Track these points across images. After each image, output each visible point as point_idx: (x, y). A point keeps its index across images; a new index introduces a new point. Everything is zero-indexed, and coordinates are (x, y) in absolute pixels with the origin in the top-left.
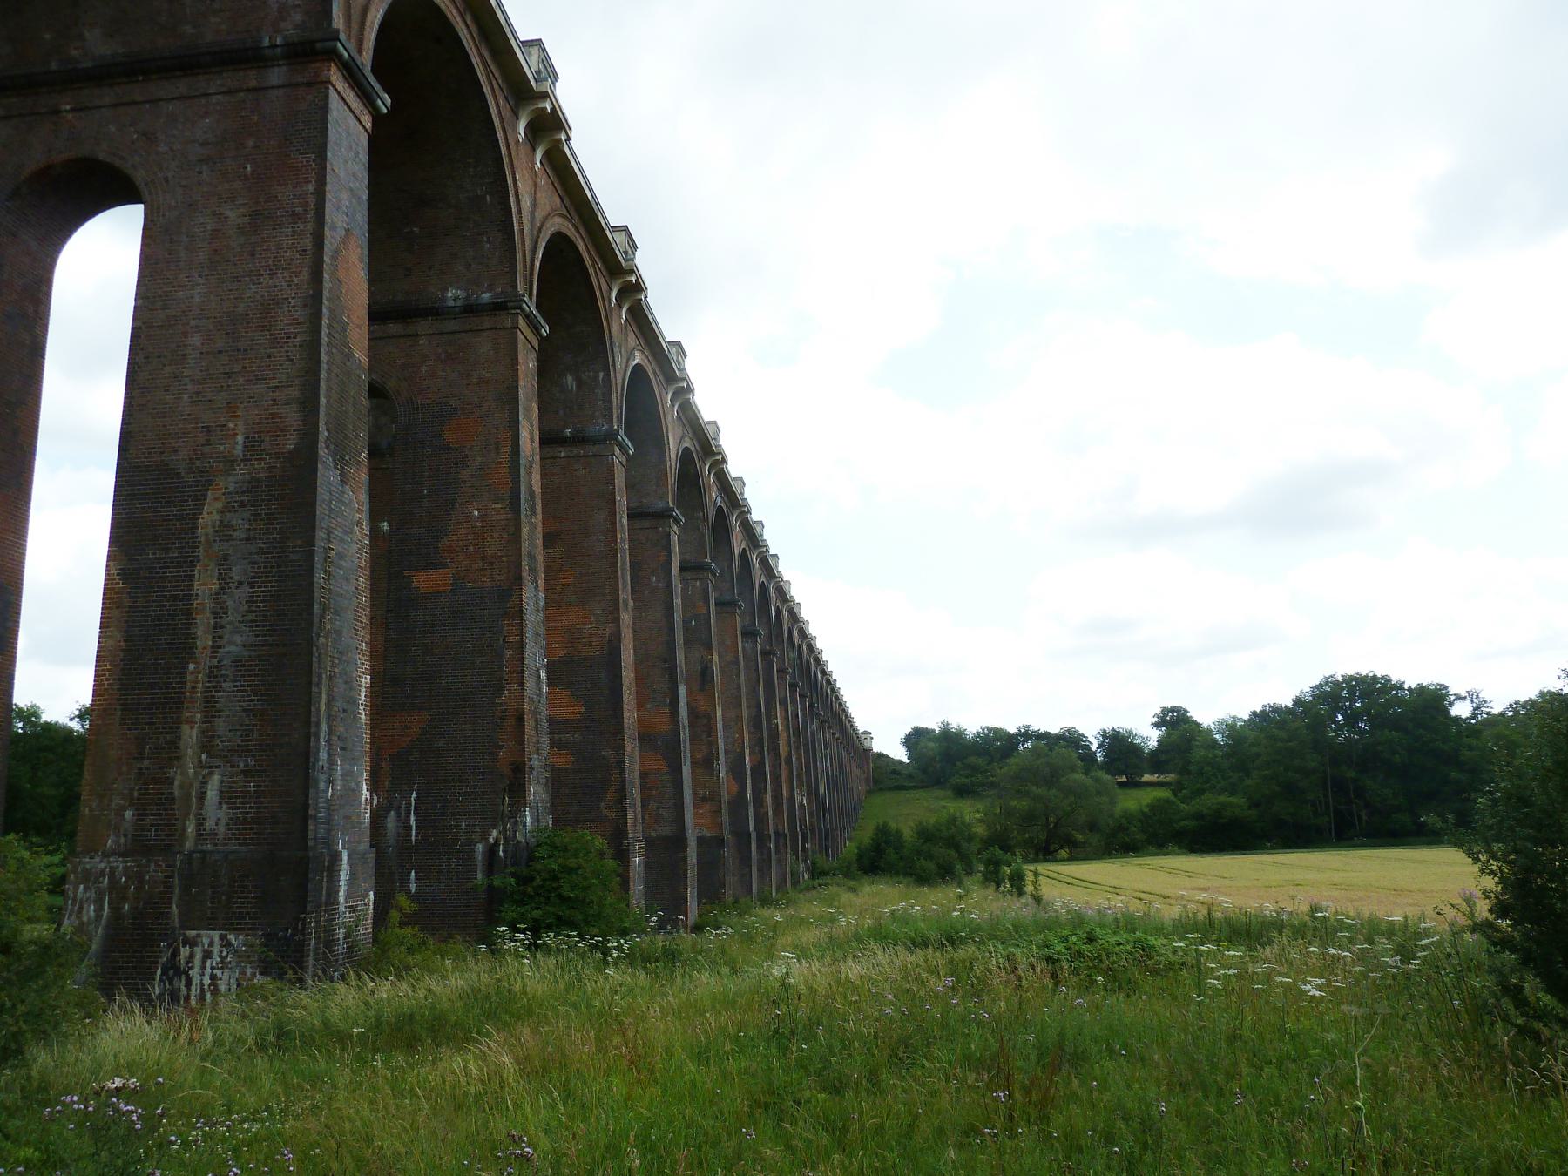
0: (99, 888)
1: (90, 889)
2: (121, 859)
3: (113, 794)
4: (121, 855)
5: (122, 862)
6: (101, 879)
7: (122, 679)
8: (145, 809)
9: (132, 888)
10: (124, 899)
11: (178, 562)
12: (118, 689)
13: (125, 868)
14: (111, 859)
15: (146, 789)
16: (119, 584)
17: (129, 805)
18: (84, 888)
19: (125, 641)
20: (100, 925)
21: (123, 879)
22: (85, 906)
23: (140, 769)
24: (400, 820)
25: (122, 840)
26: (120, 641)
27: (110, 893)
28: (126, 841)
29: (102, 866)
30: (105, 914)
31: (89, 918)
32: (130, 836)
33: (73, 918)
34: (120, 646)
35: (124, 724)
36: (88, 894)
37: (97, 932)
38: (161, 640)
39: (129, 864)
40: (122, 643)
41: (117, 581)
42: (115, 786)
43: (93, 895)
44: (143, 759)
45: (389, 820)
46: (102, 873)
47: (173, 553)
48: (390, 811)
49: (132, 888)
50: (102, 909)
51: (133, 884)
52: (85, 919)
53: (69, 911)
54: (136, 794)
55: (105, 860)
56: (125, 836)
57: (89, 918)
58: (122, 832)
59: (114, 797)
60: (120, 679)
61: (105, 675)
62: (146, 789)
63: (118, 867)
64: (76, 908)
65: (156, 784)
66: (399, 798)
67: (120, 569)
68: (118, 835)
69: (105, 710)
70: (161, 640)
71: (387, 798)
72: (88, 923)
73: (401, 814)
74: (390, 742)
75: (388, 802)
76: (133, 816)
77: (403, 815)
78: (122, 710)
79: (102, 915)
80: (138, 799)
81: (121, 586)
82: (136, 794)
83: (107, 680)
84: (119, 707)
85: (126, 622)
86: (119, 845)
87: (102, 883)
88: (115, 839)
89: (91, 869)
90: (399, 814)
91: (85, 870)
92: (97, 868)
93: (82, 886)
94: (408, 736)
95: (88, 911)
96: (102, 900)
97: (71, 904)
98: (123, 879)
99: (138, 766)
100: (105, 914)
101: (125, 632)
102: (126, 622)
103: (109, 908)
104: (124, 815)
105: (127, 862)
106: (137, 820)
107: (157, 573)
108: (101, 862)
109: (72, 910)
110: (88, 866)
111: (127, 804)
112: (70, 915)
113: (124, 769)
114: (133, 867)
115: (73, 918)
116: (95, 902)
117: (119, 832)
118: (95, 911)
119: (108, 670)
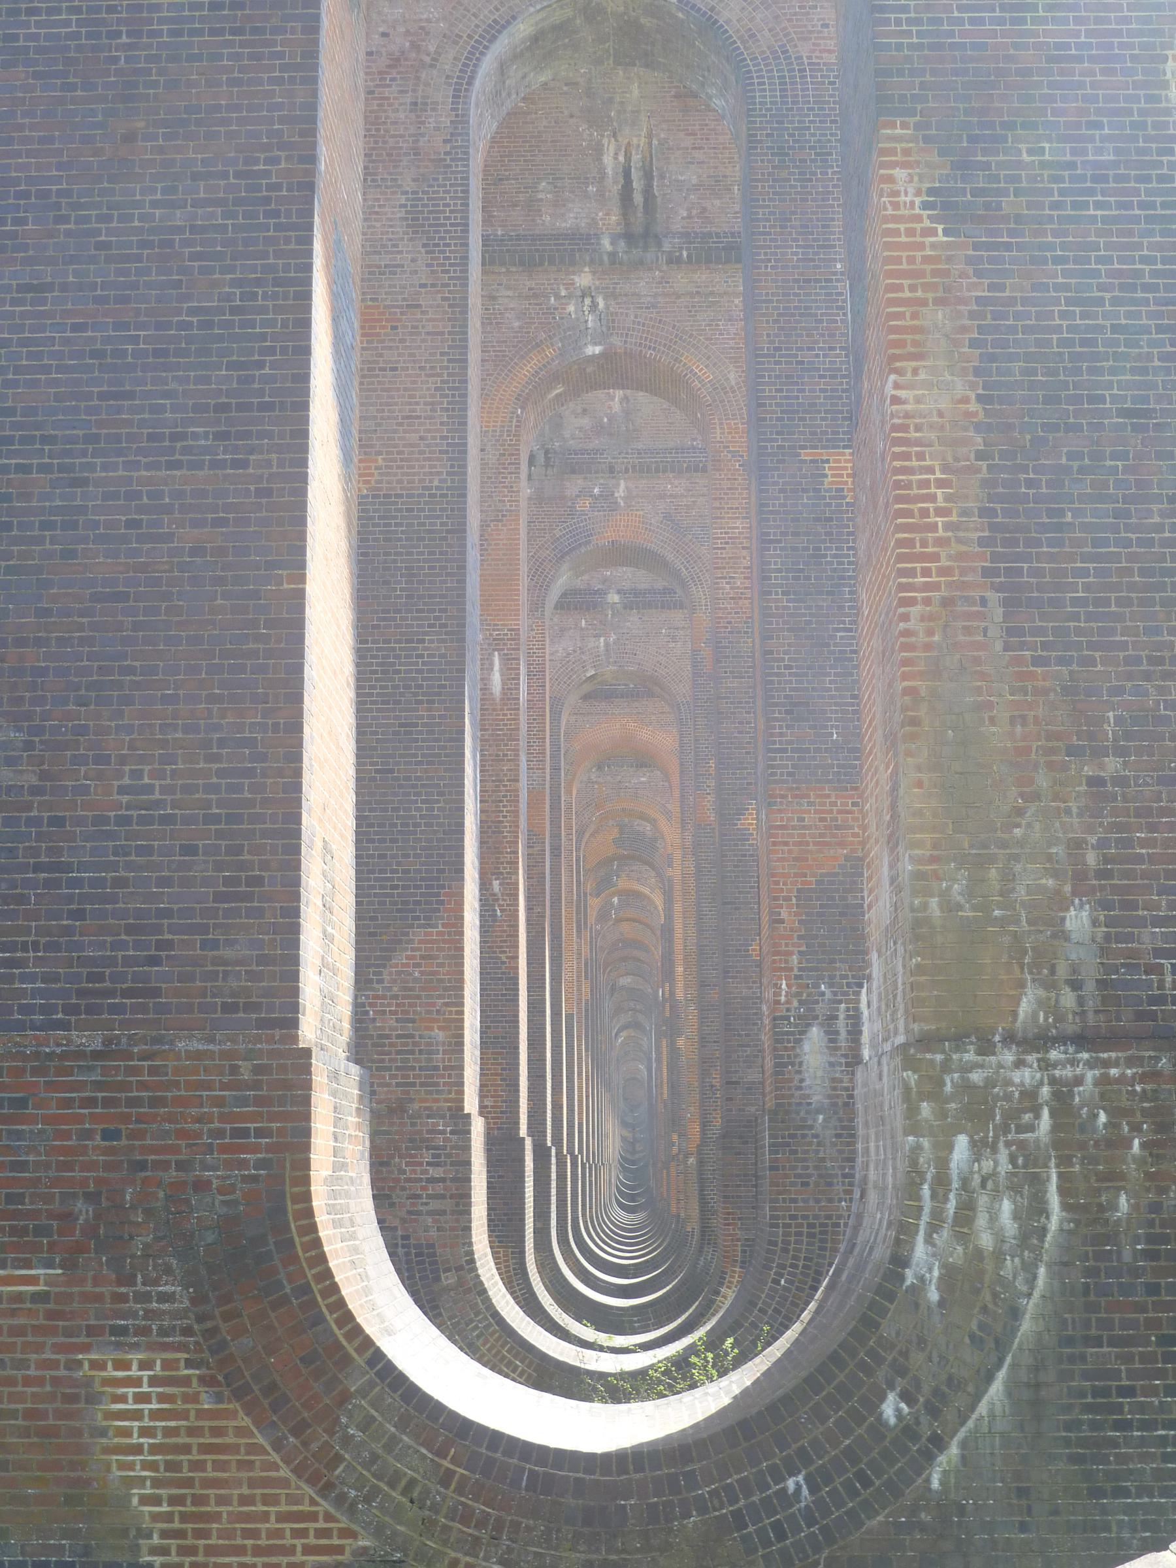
0: (1022, 1145)
1: (994, 1149)
2: (1085, 1055)
3: (1016, 858)
4: (1082, 1040)
5: (1090, 1065)
6: (1027, 1117)
7: (991, 513)
8: (1131, 906)
9: (1136, 1142)
10: (1113, 1178)
11: (1119, 178)
12: (981, 542)
13: (1103, 1081)
14: (1054, 1055)
15: (1128, 843)
16: (933, 233)
17: (1074, 893)
18: (973, 1144)
19: (980, 398)
20: (1038, 1259)
21: (1103, 1118)
22: (983, 1200)
23: (1095, 782)
24: (837, 1049)
25: (1068, 999)
26: (965, 400)
27: (1064, 1161)
28: (1081, 1001)
29: (1025, 1076)
30: (1054, 1224)
31: (1000, 1239)
32: (1090, 987)
33: (944, 1236)
34: (968, 414)
35: (1022, 646)
36: (987, 1165)
37: (1032, 1281)
38: (1102, 400)
39: (1114, 1072)
40: (973, 407)
41: (927, 223)
42: (1017, 831)
43: (1005, 1167)
44: (1099, 753)
45: (807, 1047)
46: (1030, 1095)
47: (1099, 151)
48: (809, 1025)
49: (1136, 1142)
50: (1042, 1210)
51: (1136, 1128)
52: (986, 1241)
53: (925, 1218)
54: (1091, 858)
55: (1031, 1058)
56: (1076, 985)
57: (1000, 1239)
58: (1062, 971)
59: (1018, 868)
60: (983, 512)
61: (932, 498)
62: (1128, 843)
63: (1079, 1081)
64: (951, 1206)
65: (1152, 828)
66: (828, 995)
67: (931, 192)
68: (1050, 985)
69: (947, 603)
70: (1102, 400)
71: (799, 994)
72: (998, 1256)
73: (837, 1033)
74: (796, 859)
75: (801, 1002)
76: (1095, 923)
77: (843, 1035)
78: (1006, 603)
79: (1044, 1230)
80: (1102, 874)
81: (942, 238)
82: (1091, 858)
83: (940, 512)
84: (993, 596)
85: (973, 343)
86: (1060, 1018)
87: (1031, 1128)
88: (1041, 993)
89: (990, 1083)
90: (831, 1035)
91: (966, 1087)
92: (1008, 1082)
93: (962, 1141)
94: (842, 844)
95: (993, 1218)
96: (1037, 1182)
97: (934, 1196)
98: (1103, 1118)
99: (1088, 771)
100: (1054, 1224)
101: (977, 372)
102: (973, 343)
103: (1065, 1207)
104: (1063, 919)
105: (1107, 1064)
106: (1107, 937)
107: (1056, 206)
108: (1019, 1064)
109: (938, 1216)
110: (976, 1077)
111: (1068, 888)
112: (933, 1228)
113: (1043, 781)
114: (1132, 1081)
115: (944, 1236)
116: (1015, 1189)
117: (1053, 971)
118: (1016, 1216)
119: (941, 484)
